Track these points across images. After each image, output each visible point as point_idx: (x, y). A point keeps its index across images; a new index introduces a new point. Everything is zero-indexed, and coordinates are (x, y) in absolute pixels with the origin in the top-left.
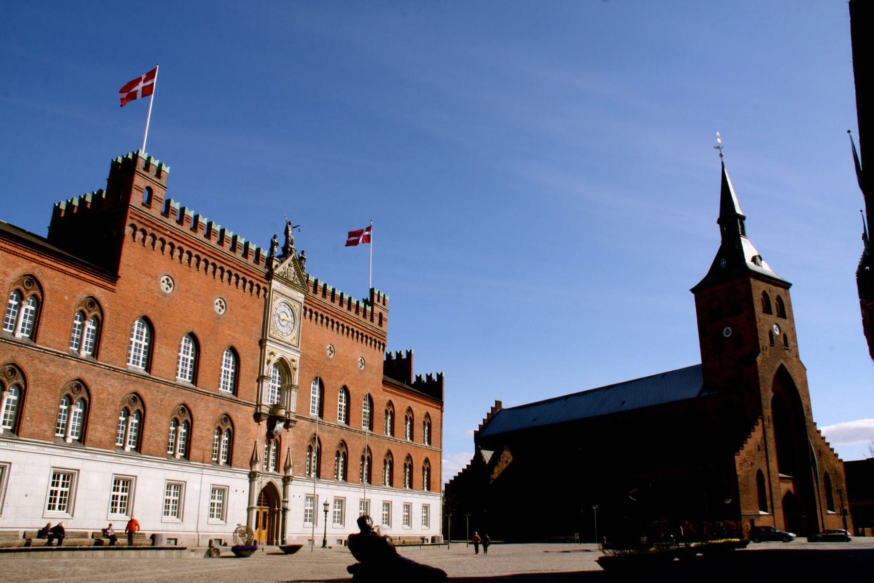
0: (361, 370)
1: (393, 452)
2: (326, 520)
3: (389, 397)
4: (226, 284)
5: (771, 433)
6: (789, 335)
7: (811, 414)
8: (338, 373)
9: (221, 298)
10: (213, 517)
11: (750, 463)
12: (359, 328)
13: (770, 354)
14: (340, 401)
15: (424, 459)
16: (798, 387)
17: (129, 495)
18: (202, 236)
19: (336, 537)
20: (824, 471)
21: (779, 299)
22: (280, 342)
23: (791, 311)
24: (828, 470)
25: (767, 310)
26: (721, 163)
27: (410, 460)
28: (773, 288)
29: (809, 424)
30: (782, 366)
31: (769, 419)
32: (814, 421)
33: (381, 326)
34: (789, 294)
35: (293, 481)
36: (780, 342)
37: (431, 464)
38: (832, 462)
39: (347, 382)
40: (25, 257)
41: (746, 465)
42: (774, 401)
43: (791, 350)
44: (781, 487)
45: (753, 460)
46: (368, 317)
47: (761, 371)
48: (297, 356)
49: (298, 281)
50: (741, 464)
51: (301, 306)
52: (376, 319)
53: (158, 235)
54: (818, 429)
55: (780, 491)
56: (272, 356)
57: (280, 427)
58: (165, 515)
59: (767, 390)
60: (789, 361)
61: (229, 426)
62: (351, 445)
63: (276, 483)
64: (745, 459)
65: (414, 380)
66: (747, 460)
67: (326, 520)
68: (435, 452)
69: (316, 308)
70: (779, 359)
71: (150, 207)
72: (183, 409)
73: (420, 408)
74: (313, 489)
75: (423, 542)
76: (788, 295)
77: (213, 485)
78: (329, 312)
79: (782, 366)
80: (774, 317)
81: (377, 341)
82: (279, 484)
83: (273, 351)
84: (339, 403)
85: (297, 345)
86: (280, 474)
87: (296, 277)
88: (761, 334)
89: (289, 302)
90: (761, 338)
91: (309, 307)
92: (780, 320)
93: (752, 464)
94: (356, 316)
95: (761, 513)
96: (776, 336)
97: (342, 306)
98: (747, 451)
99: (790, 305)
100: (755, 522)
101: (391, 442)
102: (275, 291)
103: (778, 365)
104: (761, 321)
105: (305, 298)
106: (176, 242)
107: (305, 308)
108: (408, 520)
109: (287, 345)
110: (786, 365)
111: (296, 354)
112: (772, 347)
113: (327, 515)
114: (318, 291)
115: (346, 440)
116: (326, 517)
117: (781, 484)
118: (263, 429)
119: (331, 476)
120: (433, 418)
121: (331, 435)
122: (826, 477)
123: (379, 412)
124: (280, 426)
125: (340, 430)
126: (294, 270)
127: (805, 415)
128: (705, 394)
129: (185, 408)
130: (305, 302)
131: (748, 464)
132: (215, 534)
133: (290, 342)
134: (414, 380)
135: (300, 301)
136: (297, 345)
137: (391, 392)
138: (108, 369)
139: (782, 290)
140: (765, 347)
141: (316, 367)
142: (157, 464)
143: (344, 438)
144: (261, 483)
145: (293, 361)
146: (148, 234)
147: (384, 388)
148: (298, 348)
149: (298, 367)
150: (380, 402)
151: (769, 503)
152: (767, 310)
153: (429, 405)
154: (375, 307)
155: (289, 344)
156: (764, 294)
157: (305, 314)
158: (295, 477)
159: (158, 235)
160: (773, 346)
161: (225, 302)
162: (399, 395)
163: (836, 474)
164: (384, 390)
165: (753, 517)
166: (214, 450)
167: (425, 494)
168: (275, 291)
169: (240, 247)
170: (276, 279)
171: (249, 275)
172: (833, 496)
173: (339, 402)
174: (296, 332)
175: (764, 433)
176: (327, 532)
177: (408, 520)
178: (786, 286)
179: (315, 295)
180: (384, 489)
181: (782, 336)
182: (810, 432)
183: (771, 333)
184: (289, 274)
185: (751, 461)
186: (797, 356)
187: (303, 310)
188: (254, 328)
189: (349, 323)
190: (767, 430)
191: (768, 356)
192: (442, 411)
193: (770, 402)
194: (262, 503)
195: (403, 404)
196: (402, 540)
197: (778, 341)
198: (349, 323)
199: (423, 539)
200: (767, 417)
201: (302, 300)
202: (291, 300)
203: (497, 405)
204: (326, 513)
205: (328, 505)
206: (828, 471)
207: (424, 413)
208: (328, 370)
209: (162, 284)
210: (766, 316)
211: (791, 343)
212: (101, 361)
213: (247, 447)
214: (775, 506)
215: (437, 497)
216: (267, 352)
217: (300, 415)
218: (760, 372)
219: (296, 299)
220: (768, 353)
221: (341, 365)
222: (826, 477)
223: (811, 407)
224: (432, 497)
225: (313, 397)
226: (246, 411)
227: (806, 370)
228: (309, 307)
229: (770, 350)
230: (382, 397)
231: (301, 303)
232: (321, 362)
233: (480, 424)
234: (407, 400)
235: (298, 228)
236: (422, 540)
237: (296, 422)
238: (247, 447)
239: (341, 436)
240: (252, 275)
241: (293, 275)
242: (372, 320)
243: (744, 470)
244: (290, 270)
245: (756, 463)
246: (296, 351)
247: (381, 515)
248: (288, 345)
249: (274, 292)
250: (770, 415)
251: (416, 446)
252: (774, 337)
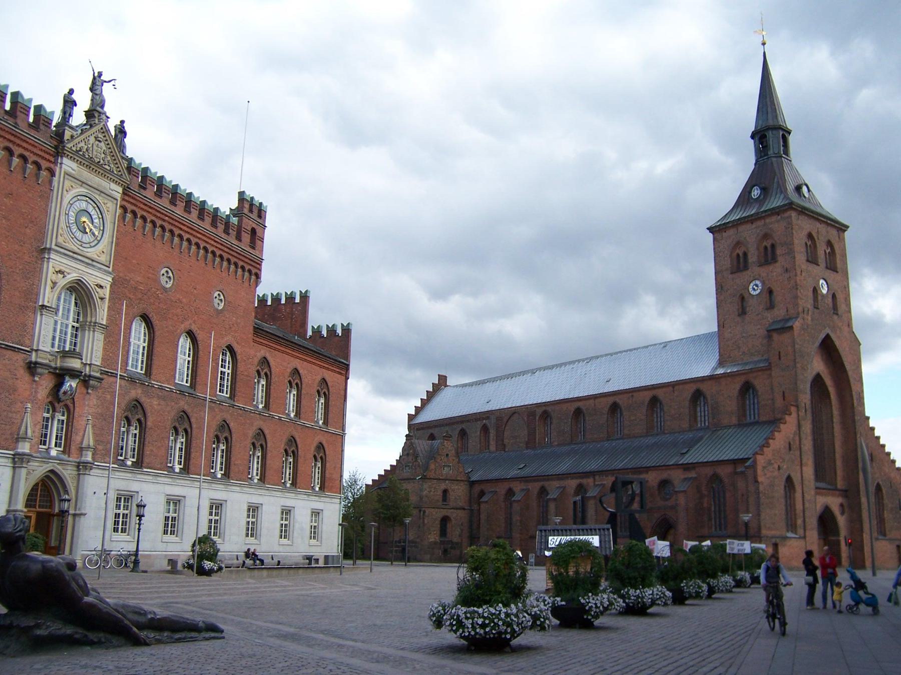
0: (217, 310)
1: (266, 432)
2: (139, 529)
3: (263, 352)
4: (224, 274)
5: (807, 427)
6: (840, 297)
7: (863, 404)
8: (179, 310)
9: (220, 291)
10: (117, 532)
11: (776, 467)
12: (216, 247)
13: (812, 320)
14: (222, 367)
15: (315, 444)
16: (848, 367)
17: (178, 516)
18: (168, 202)
19: (166, 555)
20: (876, 482)
21: (829, 244)
22: (75, 256)
23: (845, 263)
24: (882, 480)
25: (812, 260)
26: (762, 54)
27: (322, 450)
28: (822, 228)
29: (859, 418)
30: (828, 337)
31: (805, 407)
32: (867, 415)
33: (254, 248)
34: (844, 239)
35: (93, 470)
36: (828, 305)
37: (327, 453)
38: (887, 471)
39: (193, 325)
40: (293, 356)
41: (771, 470)
42: (849, 557)
43: (842, 316)
44: (817, 501)
45: (781, 462)
46: (233, 233)
47: (798, 341)
48: (107, 280)
49: (112, 166)
50: (764, 467)
51: (117, 204)
52: (246, 238)
53: (30, 157)
54: (871, 426)
55: (816, 506)
56: (60, 276)
57: (71, 386)
58: (114, 531)
59: (806, 368)
60: (838, 332)
61: (140, 416)
62: (197, 419)
63: (63, 474)
64: (770, 461)
65: (310, 333)
66: (773, 462)
67: (139, 529)
68: (334, 435)
69: (236, 257)
70: (825, 328)
71: (162, 197)
72: (135, 407)
73: (312, 373)
74: (107, 480)
75: (310, 563)
76: (842, 240)
77: (118, 490)
78: (177, 224)
79: (828, 337)
80: (820, 270)
81: (247, 269)
82: (68, 473)
83: (62, 268)
84: (220, 369)
85: (107, 264)
86: (71, 459)
87: (109, 158)
88: (802, 291)
89: (97, 197)
90: (801, 296)
91: (130, 207)
92: (829, 274)
93: (779, 468)
94: (213, 230)
95: (790, 535)
96: (823, 295)
97: (190, 212)
98: (773, 450)
99: (844, 255)
100: (780, 548)
101: (263, 417)
102: (67, 174)
103: (822, 336)
104: (803, 274)
105: (124, 193)
106: (129, 205)
107: (123, 208)
108: (285, 531)
109: (90, 262)
110: (833, 336)
111: (105, 277)
112: (815, 310)
113: (142, 522)
114: (205, 216)
115: (189, 411)
116: (140, 524)
117: (818, 497)
118: (41, 388)
119: (161, 464)
120: (332, 387)
121: (162, 403)
122: (878, 488)
123: (246, 373)
124: (71, 384)
125: (180, 396)
126: (104, 148)
127: (855, 404)
128: (720, 371)
129: (138, 404)
130: (123, 199)
131: (773, 468)
132: (422, 564)
133: (95, 257)
134: (310, 333)
135: (115, 197)
136: (108, 263)
137: (266, 346)
138: (259, 414)
139: (834, 232)
140: (806, 310)
141: (140, 299)
142: (188, 482)
143: (186, 408)
144: (38, 470)
145: (101, 287)
146: (30, 162)
147: (255, 338)
148: (109, 267)
149: (107, 296)
150: (248, 359)
151: (799, 522)
152: (812, 260)
153: (328, 369)
154: (245, 220)
155: (93, 260)
156: (810, 236)
157: (124, 218)
158: (96, 463)
159: (30, 157)
160: (817, 308)
161: (172, 273)
162: (279, 350)
163: (891, 487)
164: (254, 341)
165: (778, 541)
166: (119, 446)
167: (316, 494)
168: (67, 174)
169: (167, 192)
170: (71, 157)
171: (18, 145)
172: (886, 516)
173: (220, 368)
174: (106, 241)
175: (799, 426)
176: (140, 548)
177: (285, 531)
178: (841, 228)
179: (142, 190)
180: (251, 486)
181: (830, 296)
182: (860, 429)
183: (815, 290)
184: (95, 153)
185: (779, 463)
186: (849, 325)
187: (119, 211)
188: (28, 231)
189: (199, 238)
190: (802, 423)
191: (810, 322)
192: (347, 378)
193: (808, 385)
194: (38, 504)
195: (285, 364)
196: (276, 560)
197: (824, 302)
198: (199, 238)
199: (309, 558)
200: (804, 405)
201: (118, 196)
202: (99, 192)
203: (441, 381)
204: (140, 520)
205: (144, 506)
206: (881, 483)
207: (319, 378)
208: (161, 305)
209: (162, 277)
210: (812, 268)
211: (842, 307)
212: (154, 380)
213: (10, 415)
214: (808, 527)
215: (336, 500)
216: (51, 270)
217: (109, 371)
218: (798, 344)
219: (107, 193)
220: (810, 318)
221: (184, 300)
222: (878, 488)
223: (863, 396)
224: (327, 500)
225: (221, 372)
226: (10, 359)
227: (860, 344)
228: (130, 207)
229: (813, 313)
230: (252, 352)
231: (117, 200)
232: (149, 293)
233: (417, 405)
234: (292, 359)
235: (113, 83)
236: (308, 561)
237: (102, 379)
238: (10, 415)
239: (181, 405)
240: (25, 145)
241: (103, 155)
242: (239, 238)
243: (768, 476)
244: (97, 146)
245: (785, 467)
246: (105, 271)
247: (278, 526)
248: (91, 262)
249: (66, 176)
250: (808, 403)
251: (304, 426)
252: (820, 298)
